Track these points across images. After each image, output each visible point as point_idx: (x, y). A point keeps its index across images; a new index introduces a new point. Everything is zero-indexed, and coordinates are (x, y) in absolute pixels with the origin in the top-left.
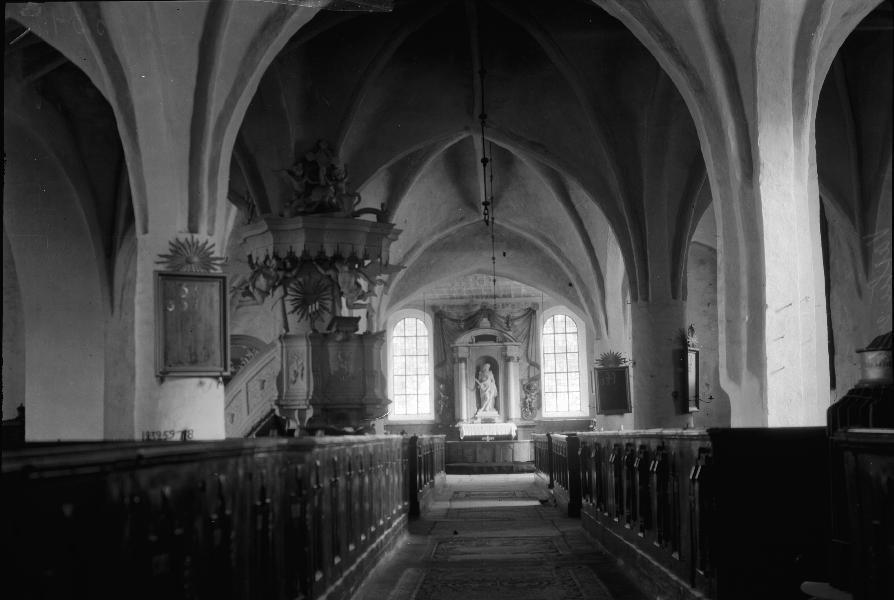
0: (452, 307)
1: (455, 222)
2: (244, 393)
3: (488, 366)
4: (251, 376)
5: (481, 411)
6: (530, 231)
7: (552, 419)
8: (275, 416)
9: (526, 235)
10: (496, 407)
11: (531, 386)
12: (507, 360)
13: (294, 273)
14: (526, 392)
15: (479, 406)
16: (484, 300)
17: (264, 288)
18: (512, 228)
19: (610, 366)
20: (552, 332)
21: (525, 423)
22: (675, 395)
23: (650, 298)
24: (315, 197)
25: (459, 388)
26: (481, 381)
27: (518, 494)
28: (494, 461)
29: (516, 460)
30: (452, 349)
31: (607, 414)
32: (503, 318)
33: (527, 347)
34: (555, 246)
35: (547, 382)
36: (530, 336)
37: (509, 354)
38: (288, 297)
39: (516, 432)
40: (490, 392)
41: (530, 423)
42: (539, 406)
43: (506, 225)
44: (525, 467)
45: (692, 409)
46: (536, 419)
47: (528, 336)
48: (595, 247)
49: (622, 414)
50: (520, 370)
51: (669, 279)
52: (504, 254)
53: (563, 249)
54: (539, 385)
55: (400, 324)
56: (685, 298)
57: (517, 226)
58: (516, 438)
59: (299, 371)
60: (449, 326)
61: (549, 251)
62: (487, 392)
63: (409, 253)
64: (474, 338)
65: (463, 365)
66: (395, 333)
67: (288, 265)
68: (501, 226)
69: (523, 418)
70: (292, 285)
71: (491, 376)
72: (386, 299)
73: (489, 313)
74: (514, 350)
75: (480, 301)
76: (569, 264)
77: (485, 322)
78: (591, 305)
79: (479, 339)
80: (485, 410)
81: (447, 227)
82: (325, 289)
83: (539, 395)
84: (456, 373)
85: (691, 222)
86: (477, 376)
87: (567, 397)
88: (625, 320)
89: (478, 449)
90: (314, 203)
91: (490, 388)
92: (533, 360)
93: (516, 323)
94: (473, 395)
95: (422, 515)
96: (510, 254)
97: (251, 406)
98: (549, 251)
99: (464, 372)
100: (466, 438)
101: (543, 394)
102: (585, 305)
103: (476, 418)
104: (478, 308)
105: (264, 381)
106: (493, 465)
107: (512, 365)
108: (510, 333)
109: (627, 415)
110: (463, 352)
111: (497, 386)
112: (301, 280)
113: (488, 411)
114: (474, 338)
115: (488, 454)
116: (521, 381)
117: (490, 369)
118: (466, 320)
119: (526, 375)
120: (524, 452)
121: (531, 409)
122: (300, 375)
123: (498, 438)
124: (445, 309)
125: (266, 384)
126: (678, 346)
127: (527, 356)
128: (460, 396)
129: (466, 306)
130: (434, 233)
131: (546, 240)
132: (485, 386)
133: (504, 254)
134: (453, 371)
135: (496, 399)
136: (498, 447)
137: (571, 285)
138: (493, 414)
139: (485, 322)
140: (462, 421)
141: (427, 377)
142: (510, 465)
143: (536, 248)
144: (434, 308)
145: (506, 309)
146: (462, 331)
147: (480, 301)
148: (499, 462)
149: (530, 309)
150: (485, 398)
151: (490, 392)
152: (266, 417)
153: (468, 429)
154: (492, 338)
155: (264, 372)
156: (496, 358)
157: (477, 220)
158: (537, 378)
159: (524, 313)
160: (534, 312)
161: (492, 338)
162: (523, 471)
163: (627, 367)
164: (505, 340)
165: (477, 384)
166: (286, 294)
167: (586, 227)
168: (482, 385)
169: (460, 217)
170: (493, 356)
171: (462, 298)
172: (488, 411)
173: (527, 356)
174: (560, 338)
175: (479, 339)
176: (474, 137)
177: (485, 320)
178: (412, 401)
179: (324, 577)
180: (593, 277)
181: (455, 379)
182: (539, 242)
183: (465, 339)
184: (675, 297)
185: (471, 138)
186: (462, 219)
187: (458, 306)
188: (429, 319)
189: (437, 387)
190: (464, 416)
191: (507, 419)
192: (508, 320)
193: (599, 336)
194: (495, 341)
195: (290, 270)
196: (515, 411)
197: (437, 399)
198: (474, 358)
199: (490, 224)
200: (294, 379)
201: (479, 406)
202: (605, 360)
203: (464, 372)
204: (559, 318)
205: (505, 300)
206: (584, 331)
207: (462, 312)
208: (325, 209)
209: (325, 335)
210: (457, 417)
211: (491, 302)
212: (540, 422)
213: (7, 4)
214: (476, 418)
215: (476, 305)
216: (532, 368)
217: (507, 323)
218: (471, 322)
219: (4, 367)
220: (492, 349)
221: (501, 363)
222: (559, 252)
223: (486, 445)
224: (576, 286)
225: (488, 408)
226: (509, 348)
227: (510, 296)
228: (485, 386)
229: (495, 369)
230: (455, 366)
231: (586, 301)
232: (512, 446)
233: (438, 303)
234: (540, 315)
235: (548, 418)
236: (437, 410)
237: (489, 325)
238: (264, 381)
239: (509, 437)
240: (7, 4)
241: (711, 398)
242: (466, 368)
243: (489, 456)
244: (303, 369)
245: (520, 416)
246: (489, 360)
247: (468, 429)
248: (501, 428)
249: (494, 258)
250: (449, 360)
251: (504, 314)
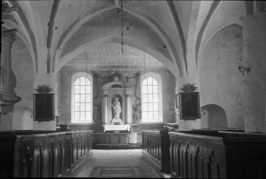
0: (101, 72)
1: (100, 8)
3: (118, 99)
5: (114, 119)
6: (143, 15)
7: (145, 123)
9: (141, 18)
10: (121, 117)
11: (137, 109)
12: (127, 96)
14: (134, 111)
15: (113, 117)
16: (116, 69)
18: (134, 14)
19: (189, 91)
21: (134, 125)
25: (104, 110)
26: (114, 106)
28: (119, 143)
29: (130, 142)
30: (101, 91)
31: (186, 119)
32: (125, 77)
33: (136, 91)
34: (157, 24)
35: (144, 107)
36: (137, 86)
37: (127, 93)
39: (130, 129)
40: (118, 111)
41: (136, 125)
42: (141, 117)
43: (129, 11)
44: (134, 146)
47: (136, 86)
48: (181, 23)
49: (194, 119)
52: (128, 29)
53: (161, 25)
54: (141, 108)
55: (78, 80)
57: (135, 12)
58: (130, 132)
60: (101, 80)
61: (153, 27)
62: (117, 111)
64: (113, 84)
65: (106, 98)
66: (76, 83)
68: (126, 12)
69: (133, 123)
71: (119, 103)
72: (59, 52)
73: (119, 75)
74: (129, 92)
75: (114, 69)
76: (164, 34)
77: (117, 78)
79: (114, 86)
80: (116, 119)
81: (95, 11)
83: (141, 112)
84: (103, 102)
86: (112, 103)
88: (197, 67)
89: (112, 137)
91: (118, 109)
92: (138, 96)
93: (131, 80)
94: (111, 111)
96: (131, 28)
98: (153, 27)
99: (106, 101)
100: (107, 132)
101: (142, 112)
103: (112, 123)
104: (114, 73)
106: (119, 145)
107: (128, 98)
108: (128, 84)
109: (197, 120)
110: (106, 92)
111: (122, 109)
114: (113, 84)
115: (116, 139)
116: (133, 106)
117: (118, 100)
118: (108, 78)
119: (135, 103)
120: (134, 139)
121: (137, 119)
123: (121, 132)
124: (99, 73)
127: (135, 95)
128: (104, 113)
129: (108, 72)
130: (87, 14)
131: (152, 21)
132: (116, 107)
133: (128, 29)
134: (101, 101)
135: (121, 114)
136: (122, 136)
137: (165, 47)
138: (119, 120)
139: (117, 78)
140: (105, 123)
142: (127, 145)
143: (146, 26)
145: (126, 73)
146: (106, 82)
147: (114, 69)
148: (122, 144)
149: (137, 74)
150: (116, 113)
153: (108, 128)
154: (120, 86)
158: (140, 105)
159: (133, 75)
160: (139, 75)
161: (120, 86)
162: (133, 148)
163: (198, 92)
164: (126, 87)
165: (112, 107)
167: (177, 10)
168: (114, 107)
169: (103, 5)
171: (106, 67)
173: (135, 95)
175: (114, 86)
177: (117, 78)
179: (73, 165)
180: (179, 42)
181: (102, 105)
182: (148, 22)
183: (108, 86)
186: (104, 7)
187: (104, 71)
188: (91, 77)
189: (94, 108)
190: (106, 121)
191: (126, 123)
192: (127, 78)
194: (121, 88)
196: (130, 119)
197: (94, 114)
198: (112, 95)
199: (120, 11)
201: (113, 117)
203: (106, 101)
204: (150, 79)
205: (125, 69)
206: (161, 84)
207: (106, 74)
210: (103, 122)
211: (120, 70)
212: (140, 124)
214: (112, 123)
215: (113, 71)
216: (138, 100)
217: (127, 79)
218: (110, 79)
220: (119, 91)
221: (123, 98)
223: (116, 135)
224: (169, 47)
225: (117, 118)
226: (127, 90)
227: (128, 68)
229: (121, 100)
230: (103, 98)
231: (174, 55)
232: (128, 136)
233: (95, 70)
234: (142, 77)
235: (73, 124)
236: (94, 119)
239: (127, 131)
242: (107, 100)
243: (117, 141)
245: (132, 122)
246: (118, 96)
247: (108, 128)
248: (127, 127)
249: (122, 34)
250: (100, 96)
251: (125, 76)
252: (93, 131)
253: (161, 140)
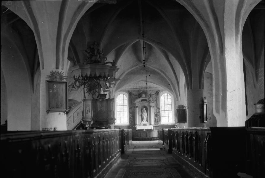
0: (134, 91)
1: (135, 66)
2: (72, 117)
3: (145, 109)
4: (74, 112)
5: (143, 122)
6: (157, 68)
7: (164, 124)
8: (82, 124)
9: (156, 70)
10: (147, 121)
11: (158, 115)
12: (150, 107)
13: (87, 81)
14: (156, 116)
15: (142, 120)
16: (143, 89)
17: (78, 85)
18: (152, 68)
19: (181, 109)
20: (164, 98)
21: (155, 125)
22: (200, 117)
23: (193, 88)
24: (93, 58)
25: (136, 115)
26: (143, 113)
27: (153, 147)
28: (146, 137)
29: (153, 136)
30: (134, 104)
31: (180, 123)
32: (149, 94)
33: (156, 103)
34: (164, 73)
35: (162, 113)
36: (157, 100)
37: (151, 105)
38: (85, 88)
39: (153, 128)
40: (145, 116)
41: (157, 125)
42: (160, 120)
43: (150, 67)
44: (156, 139)
45: (205, 121)
46: (159, 124)
47: (156, 100)
48: (176, 73)
49: (184, 123)
50: (154, 110)
51: (198, 83)
52: (149, 75)
53: (167, 74)
54: (160, 114)
55: (119, 96)
56: (203, 88)
57: (153, 67)
58: (153, 130)
59: (89, 110)
60: (133, 97)
61: (163, 74)
62: (144, 116)
63: (121, 75)
64: (140, 100)
65: (137, 108)
66: (117, 99)
67: (85, 78)
68: (148, 67)
69: (155, 124)
70: (87, 85)
71: (145, 111)
72: (115, 89)
73: (145, 93)
74: (152, 104)
75: (142, 89)
76: (169, 78)
77: (144, 95)
78: (175, 90)
79: (142, 100)
80: (144, 122)
81: (132, 67)
82: (96, 86)
83: (160, 117)
84: (135, 111)
85: (205, 66)
86: (141, 112)
87: (168, 118)
88: (185, 95)
89: (142, 133)
90: (93, 60)
91: (145, 115)
92: (158, 107)
93: (153, 96)
94: (140, 117)
95: (125, 153)
96: (151, 75)
97: (74, 120)
98: (163, 74)
99: (137, 110)
100: (138, 130)
101: (161, 117)
102: (173, 90)
103: (141, 124)
104: (142, 91)
105: (78, 113)
106: (146, 138)
107: (152, 108)
108: (151, 99)
109: (186, 123)
110: (137, 105)
111: (147, 115)
112: (89, 83)
113: (145, 122)
114: (140, 100)
115: (145, 135)
116: (155, 113)
117: (145, 110)
118: (138, 95)
119: (156, 111)
120: (155, 134)
121: (157, 121)
122: (89, 111)
123: (147, 130)
124: (132, 92)
125: (79, 114)
126: (201, 103)
127: (156, 106)
128: (136, 117)
129: (138, 91)
130: (129, 69)
131: (162, 71)
132: (144, 114)
133: (149, 75)
134: (134, 110)
135: (147, 118)
136: (148, 133)
137: (169, 84)
138: (146, 123)
139: (144, 95)
140: (137, 125)
141: (127, 112)
142: (151, 138)
143: (159, 74)
144: (129, 91)
145: (150, 92)
146: (137, 98)
147: (142, 89)
148: (148, 137)
149: (157, 92)
150: (144, 118)
151: (145, 116)
152: (79, 124)
153: (139, 127)
154: (146, 100)
155: (78, 110)
156: (147, 106)
157: (141, 65)
158: (159, 112)
159: (155, 93)
160: (158, 93)
161: (146, 100)
162: (155, 140)
163: (186, 109)
164: (150, 101)
165: (141, 114)
166: (85, 87)
167: (174, 67)
168: (143, 114)
169: (136, 64)
170: (146, 105)
171: (137, 88)
172: (145, 122)
173: (156, 106)
174: (166, 100)
175: (142, 100)
176: (141, 41)
177: (144, 95)
178: (122, 119)
179: (96, 171)
180: (176, 82)
181: (135, 113)
182: (160, 72)
183: (138, 100)
184: (200, 88)
185: (140, 41)
186: (137, 65)
187: (136, 91)
188: (127, 95)
189: (129, 115)
190: (138, 124)
191: (150, 124)
192: (151, 95)
193: (178, 100)
194: (147, 101)
195: (86, 80)
196: (153, 122)
197: (130, 118)
198: (141, 106)
199: (145, 66)
200: (87, 112)
201: (142, 120)
202: (179, 107)
203: (137, 110)
204: (166, 94)
205: (150, 89)
206: (173, 98)
207: (137, 93)
208: (96, 62)
209: (96, 99)
210: (135, 124)
211: (146, 89)
212: (160, 125)
213: (2, 1)
214: (141, 124)
215: (141, 90)
216: (158, 109)
217: (150, 96)
218: (140, 96)
219: (1, 109)
220: (146, 104)
221: (148, 108)
222: (166, 75)
223: (144, 132)
224: (171, 85)
225: (145, 121)
226: (151, 103)
227: (151, 88)
228: (144, 114)
229: (147, 110)
230: (135, 109)
231: (174, 89)
232: (152, 132)
233: (130, 90)
234: (160, 94)
236: (129, 122)
237: (145, 96)
238: (78, 113)
239: (151, 130)
240: (2, 1)
241: (211, 118)
242: (138, 109)
243: (145, 135)
244: (90, 109)
245: (154, 124)
246: (145, 107)
247: (139, 127)
248: (149, 127)
249: (146, 77)
250: (133, 107)
251: (149, 93)
252: (264, 128)
253: (168, 136)
